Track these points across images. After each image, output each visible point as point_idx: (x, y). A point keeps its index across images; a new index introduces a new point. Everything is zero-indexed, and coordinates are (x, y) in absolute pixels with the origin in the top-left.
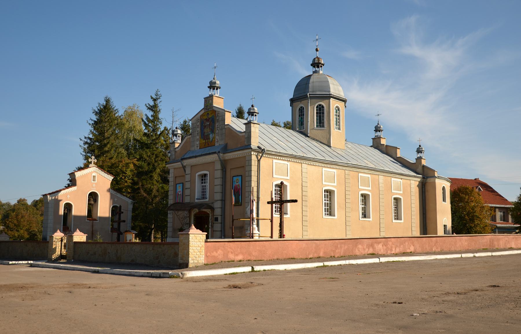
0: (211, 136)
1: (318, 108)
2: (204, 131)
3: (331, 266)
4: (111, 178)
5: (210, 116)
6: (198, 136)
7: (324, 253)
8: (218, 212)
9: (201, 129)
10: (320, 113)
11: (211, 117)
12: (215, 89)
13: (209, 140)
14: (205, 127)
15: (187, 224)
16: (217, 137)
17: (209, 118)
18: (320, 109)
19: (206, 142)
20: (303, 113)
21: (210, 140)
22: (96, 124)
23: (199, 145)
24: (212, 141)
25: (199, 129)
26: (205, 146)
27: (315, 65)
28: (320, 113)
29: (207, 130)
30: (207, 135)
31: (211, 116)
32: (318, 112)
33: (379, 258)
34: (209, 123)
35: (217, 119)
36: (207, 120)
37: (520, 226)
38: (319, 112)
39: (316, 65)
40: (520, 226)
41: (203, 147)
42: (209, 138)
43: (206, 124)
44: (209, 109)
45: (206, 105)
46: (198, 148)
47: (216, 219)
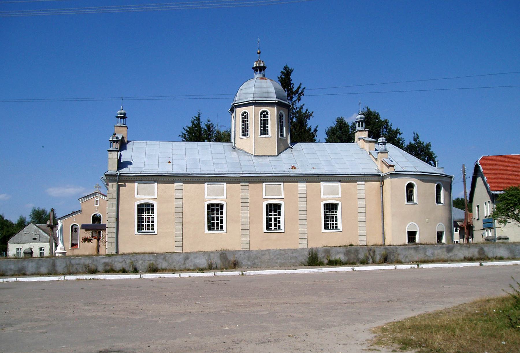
28: (245, 121)
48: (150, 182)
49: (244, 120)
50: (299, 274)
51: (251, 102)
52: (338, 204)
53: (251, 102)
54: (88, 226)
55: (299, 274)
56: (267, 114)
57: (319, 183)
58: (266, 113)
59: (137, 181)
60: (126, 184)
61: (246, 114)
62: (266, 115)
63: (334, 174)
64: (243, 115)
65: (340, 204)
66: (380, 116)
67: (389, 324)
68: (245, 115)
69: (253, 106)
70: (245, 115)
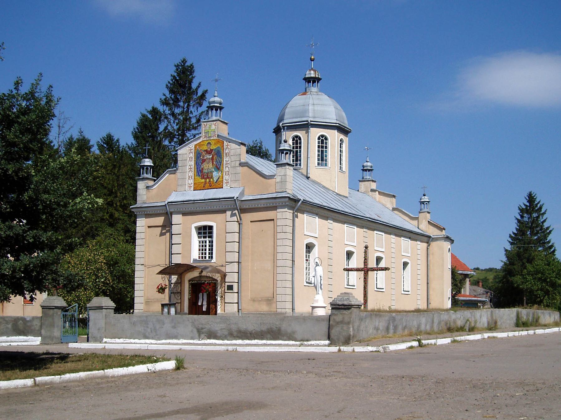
0: (216, 175)
1: (320, 140)
2: (202, 167)
3: (293, 341)
4: (363, 267)
5: (213, 147)
6: (190, 172)
7: (102, 312)
8: (231, 278)
9: (197, 164)
10: (322, 147)
11: (216, 149)
12: (213, 110)
13: (211, 180)
14: (204, 161)
15: (178, 293)
16: (226, 177)
17: (212, 150)
18: (322, 141)
19: (206, 182)
20: (299, 145)
21: (213, 179)
22: (515, 239)
23: (193, 184)
24: (217, 181)
25: (193, 163)
26: (204, 187)
27: (311, 80)
28: (322, 147)
29: (208, 166)
30: (208, 173)
31: (215, 148)
32: (320, 145)
33: (508, 336)
34: (211, 157)
35: (226, 152)
36: (209, 152)
37: (29, 226)
38: (321, 146)
39: (312, 80)
40: (29, 227)
41: (202, 189)
42: (212, 177)
43: (205, 158)
44: (211, 137)
45: (206, 131)
46: (192, 189)
47: (230, 288)
48: (312, 214)
49: (320, 145)
50: (301, 353)
51: (335, 125)
52: (195, 227)
53: (335, 125)
54: (553, 334)
55: (301, 353)
56: (300, 139)
57: (373, 232)
58: (324, 138)
59: (307, 213)
60: (298, 213)
61: (323, 139)
62: (324, 141)
63: (381, 221)
64: (319, 138)
65: (194, 226)
66: (120, 143)
67: (73, 319)
68: (296, 139)
69: (336, 131)
70: (296, 139)
